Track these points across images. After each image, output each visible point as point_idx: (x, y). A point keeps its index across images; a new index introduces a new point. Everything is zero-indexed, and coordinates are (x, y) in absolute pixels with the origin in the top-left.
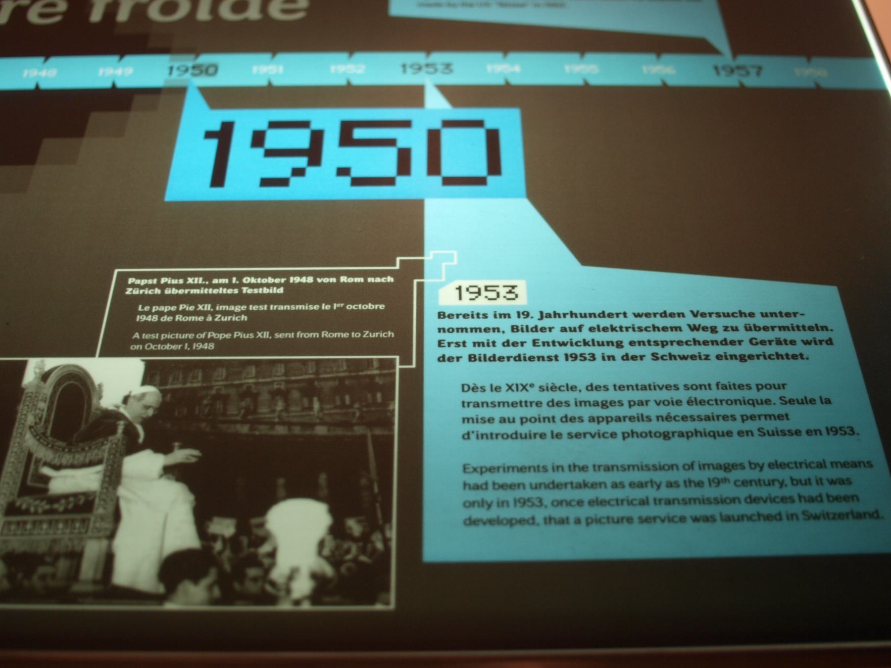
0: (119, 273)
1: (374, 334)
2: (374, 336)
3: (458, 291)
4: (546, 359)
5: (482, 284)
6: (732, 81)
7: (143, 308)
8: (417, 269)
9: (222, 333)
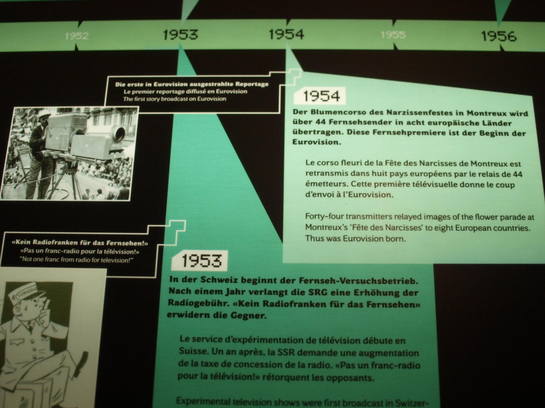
0: (110, 78)
1: (204, 98)
2: (204, 100)
3: (305, 95)
4: (392, 133)
5: (319, 90)
6: (493, 46)
7: (126, 92)
8: (282, 79)
9: (175, 101)
